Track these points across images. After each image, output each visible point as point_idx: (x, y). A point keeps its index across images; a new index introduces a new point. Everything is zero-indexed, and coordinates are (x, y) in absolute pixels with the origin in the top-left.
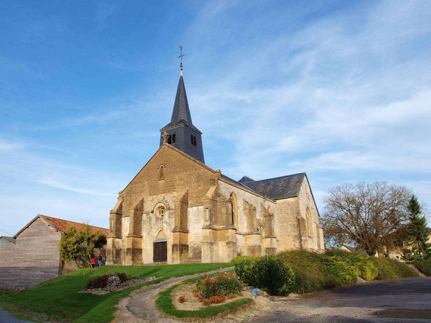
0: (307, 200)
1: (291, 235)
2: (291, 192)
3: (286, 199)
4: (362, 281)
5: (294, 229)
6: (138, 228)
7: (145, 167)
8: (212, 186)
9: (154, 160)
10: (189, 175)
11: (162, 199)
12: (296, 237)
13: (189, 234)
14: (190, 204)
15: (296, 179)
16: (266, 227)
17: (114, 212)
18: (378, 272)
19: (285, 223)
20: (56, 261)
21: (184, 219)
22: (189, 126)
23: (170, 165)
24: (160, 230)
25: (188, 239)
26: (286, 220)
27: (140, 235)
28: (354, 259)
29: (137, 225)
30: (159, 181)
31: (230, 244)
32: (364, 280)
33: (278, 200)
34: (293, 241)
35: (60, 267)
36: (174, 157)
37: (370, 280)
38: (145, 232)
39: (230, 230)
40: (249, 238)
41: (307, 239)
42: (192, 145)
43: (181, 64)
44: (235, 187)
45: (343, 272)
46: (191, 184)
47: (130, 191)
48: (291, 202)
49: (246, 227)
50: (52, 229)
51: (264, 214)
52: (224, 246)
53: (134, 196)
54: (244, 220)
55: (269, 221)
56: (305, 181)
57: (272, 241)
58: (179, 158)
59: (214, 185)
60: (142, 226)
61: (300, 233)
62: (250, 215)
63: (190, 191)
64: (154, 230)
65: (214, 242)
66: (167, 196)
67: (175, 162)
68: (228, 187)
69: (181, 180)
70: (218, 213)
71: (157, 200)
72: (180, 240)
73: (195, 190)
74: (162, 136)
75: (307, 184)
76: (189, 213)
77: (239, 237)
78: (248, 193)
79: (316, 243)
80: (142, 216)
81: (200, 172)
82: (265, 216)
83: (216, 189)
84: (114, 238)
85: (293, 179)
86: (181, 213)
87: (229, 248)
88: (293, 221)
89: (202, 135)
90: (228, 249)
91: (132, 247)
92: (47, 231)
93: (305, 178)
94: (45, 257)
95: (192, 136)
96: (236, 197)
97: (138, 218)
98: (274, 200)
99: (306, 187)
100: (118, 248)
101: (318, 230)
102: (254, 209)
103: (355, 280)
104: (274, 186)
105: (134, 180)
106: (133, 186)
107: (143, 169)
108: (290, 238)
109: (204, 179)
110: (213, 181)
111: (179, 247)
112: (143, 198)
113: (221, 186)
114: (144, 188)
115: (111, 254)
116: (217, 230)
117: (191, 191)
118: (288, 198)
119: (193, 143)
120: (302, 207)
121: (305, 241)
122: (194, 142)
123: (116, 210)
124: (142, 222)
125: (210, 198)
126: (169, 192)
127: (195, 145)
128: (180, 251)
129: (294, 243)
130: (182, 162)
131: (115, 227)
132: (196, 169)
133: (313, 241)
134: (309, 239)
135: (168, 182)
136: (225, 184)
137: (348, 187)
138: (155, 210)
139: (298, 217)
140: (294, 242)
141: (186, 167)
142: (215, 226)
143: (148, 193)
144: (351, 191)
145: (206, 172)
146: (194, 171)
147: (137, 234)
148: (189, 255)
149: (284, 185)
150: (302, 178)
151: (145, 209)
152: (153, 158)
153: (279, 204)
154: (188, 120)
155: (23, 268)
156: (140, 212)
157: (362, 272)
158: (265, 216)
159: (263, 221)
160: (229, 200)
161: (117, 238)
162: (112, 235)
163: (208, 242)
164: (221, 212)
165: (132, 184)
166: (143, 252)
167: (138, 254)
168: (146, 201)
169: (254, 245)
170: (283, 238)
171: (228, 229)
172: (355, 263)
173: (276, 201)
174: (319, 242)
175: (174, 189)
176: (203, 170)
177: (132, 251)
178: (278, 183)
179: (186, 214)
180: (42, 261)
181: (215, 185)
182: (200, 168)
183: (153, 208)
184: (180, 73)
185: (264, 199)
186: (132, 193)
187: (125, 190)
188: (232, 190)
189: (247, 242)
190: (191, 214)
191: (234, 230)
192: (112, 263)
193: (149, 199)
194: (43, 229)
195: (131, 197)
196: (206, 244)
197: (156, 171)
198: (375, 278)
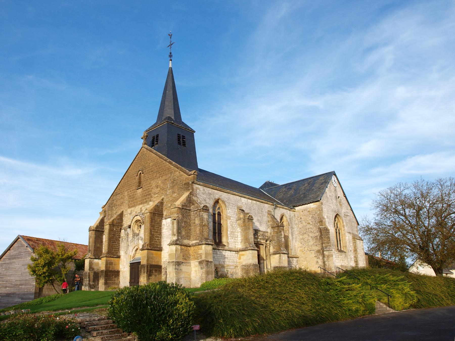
1: (313, 250)
3: (306, 205)
6: (115, 246)
7: (125, 175)
8: (186, 191)
9: (134, 166)
10: (165, 180)
11: (139, 211)
12: (318, 251)
13: (163, 252)
14: (165, 216)
15: (322, 180)
16: (274, 240)
17: (92, 229)
18: (416, 297)
19: (306, 235)
20: (32, 286)
22: (175, 123)
24: (136, 248)
25: (162, 258)
26: (306, 231)
27: (118, 255)
28: (380, 280)
30: (138, 190)
31: (203, 264)
32: (392, 309)
33: (297, 206)
34: (315, 257)
35: (35, 293)
36: (151, 161)
37: (400, 308)
38: (123, 250)
39: (204, 246)
40: (243, 255)
43: (171, 53)
44: (223, 192)
45: (348, 300)
46: (166, 191)
47: (112, 204)
48: (313, 208)
49: (240, 241)
50: (30, 250)
51: (271, 224)
52: (197, 267)
54: (238, 232)
55: (277, 233)
56: (333, 181)
57: (281, 258)
58: (156, 161)
60: (120, 244)
61: (322, 246)
62: (244, 226)
63: (165, 200)
64: (131, 248)
65: (183, 261)
68: (210, 192)
69: (157, 187)
70: (192, 225)
71: (135, 212)
72: (148, 260)
73: (170, 198)
75: (336, 185)
77: (229, 254)
78: (245, 199)
79: (351, 259)
80: (120, 232)
81: (175, 176)
82: (272, 227)
83: (189, 195)
84: (92, 258)
85: (319, 181)
86: (151, 227)
87: (202, 268)
88: (315, 232)
89: (194, 134)
90: (200, 269)
91: (106, 269)
92: (25, 253)
94: (23, 282)
96: (225, 205)
97: (115, 235)
98: (292, 207)
100: (97, 270)
101: (355, 242)
102: (250, 218)
103: (372, 309)
104: (296, 190)
105: (116, 191)
106: (114, 198)
107: (124, 178)
108: (312, 253)
109: (179, 184)
110: (187, 186)
111: (146, 268)
112: (123, 212)
113: (198, 191)
114: (124, 199)
115: (88, 277)
116: (190, 246)
117: (166, 200)
118: (309, 203)
119: (180, 143)
120: (326, 214)
121: (328, 256)
122: (181, 142)
123: (95, 226)
125: (177, 206)
127: (184, 145)
128: (147, 273)
129: (316, 260)
130: (159, 166)
131: (93, 246)
132: (172, 172)
135: (145, 190)
136: (205, 188)
137: (402, 188)
138: (132, 225)
140: (316, 258)
142: (186, 242)
143: (127, 205)
144: (406, 192)
145: (182, 175)
146: (169, 175)
147: (112, 254)
148: (162, 277)
149: (307, 188)
150: (329, 178)
151: (124, 224)
152: (133, 164)
153: (298, 211)
155: (4, 295)
156: (118, 228)
157: (388, 297)
159: (270, 234)
160: (204, 208)
162: (89, 255)
163: (173, 262)
164: (195, 223)
166: (121, 274)
167: (113, 277)
169: (248, 263)
170: (304, 253)
171: (201, 245)
172: (379, 286)
173: (295, 208)
175: (151, 198)
176: (178, 173)
177: (105, 274)
179: (159, 228)
180: (20, 287)
182: (175, 171)
184: (172, 65)
185: (274, 206)
186: (113, 206)
187: (107, 204)
188: (217, 195)
189: (241, 260)
190: (165, 228)
191: (211, 246)
192: (88, 288)
193: (128, 212)
194: (23, 251)
195: (112, 211)
196: (172, 264)
197: (135, 179)
198: (411, 306)
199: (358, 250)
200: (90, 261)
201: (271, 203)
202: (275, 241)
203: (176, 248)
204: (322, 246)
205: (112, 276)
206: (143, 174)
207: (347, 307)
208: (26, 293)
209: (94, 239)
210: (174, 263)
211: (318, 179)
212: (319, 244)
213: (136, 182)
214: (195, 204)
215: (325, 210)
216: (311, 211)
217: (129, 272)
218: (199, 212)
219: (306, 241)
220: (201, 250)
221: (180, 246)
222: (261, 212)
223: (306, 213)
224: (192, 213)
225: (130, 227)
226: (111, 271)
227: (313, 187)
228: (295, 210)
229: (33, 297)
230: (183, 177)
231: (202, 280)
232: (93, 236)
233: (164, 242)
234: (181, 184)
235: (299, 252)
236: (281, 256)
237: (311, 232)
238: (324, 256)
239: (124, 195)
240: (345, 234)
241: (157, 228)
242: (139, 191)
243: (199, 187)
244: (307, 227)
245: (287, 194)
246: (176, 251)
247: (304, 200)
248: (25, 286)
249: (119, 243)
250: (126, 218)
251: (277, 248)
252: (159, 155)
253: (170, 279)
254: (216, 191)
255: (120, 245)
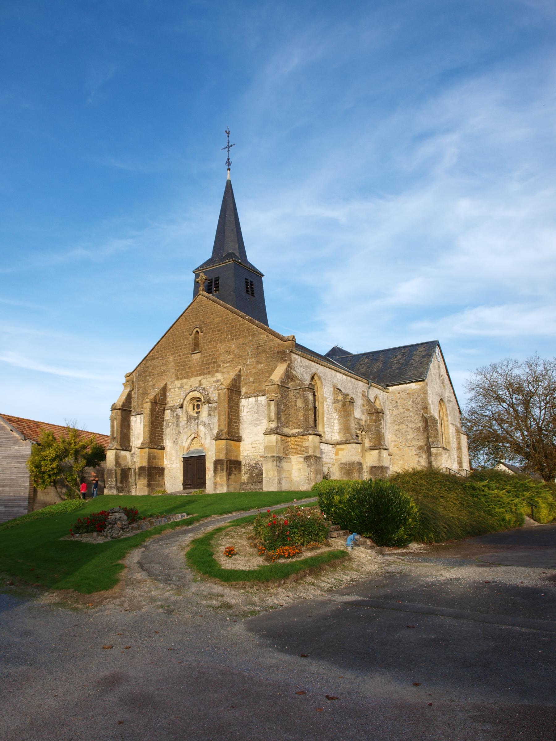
0: (440, 387)
1: (413, 446)
2: (413, 372)
3: (405, 385)
4: (533, 524)
5: (417, 435)
6: (158, 433)
7: (169, 332)
8: (281, 362)
11: (197, 385)
12: (421, 448)
13: (242, 443)
14: (244, 393)
17: (118, 407)
19: (403, 425)
21: (233, 418)
22: (242, 263)
23: (210, 329)
24: (193, 437)
25: (241, 451)
26: (404, 420)
28: (520, 487)
29: (155, 428)
30: (193, 355)
31: (310, 460)
32: (536, 523)
34: (416, 455)
36: (217, 315)
37: (545, 521)
38: (168, 439)
39: (311, 437)
40: (342, 449)
41: (440, 453)
42: (247, 294)
43: (228, 159)
44: (319, 364)
45: (500, 508)
46: (245, 359)
47: (145, 372)
48: (414, 389)
49: (338, 431)
51: (367, 410)
53: (150, 380)
55: (376, 421)
57: (381, 455)
59: (284, 361)
60: (164, 430)
61: (428, 441)
62: (344, 411)
64: (183, 437)
65: (284, 456)
66: (205, 380)
67: (219, 323)
68: (307, 364)
69: (229, 353)
70: (291, 408)
71: (189, 387)
72: (226, 453)
73: (252, 370)
74: (197, 280)
75: (440, 359)
76: (242, 408)
78: (341, 375)
79: (454, 459)
80: (164, 413)
81: (261, 340)
82: (369, 414)
85: (418, 352)
86: (229, 408)
87: (308, 466)
88: (417, 421)
89: (263, 278)
90: (306, 467)
92: (8, 439)
93: (437, 350)
95: (246, 279)
96: (321, 381)
97: (158, 417)
99: (439, 364)
100: (125, 466)
101: (459, 438)
102: (351, 401)
104: (384, 363)
105: (151, 354)
106: (149, 363)
107: (166, 335)
108: (411, 450)
109: (268, 352)
110: (282, 355)
111: (225, 464)
112: (166, 384)
113: (296, 362)
115: (114, 476)
116: (289, 437)
117: (245, 372)
118: (409, 383)
119: (249, 291)
121: (436, 455)
122: (250, 290)
123: (121, 404)
124: (165, 423)
125: (277, 383)
126: (209, 373)
127: (253, 294)
128: (226, 471)
129: (417, 459)
130: (231, 323)
131: (119, 432)
133: (449, 455)
134: (443, 452)
136: (302, 359)
137: (511, 366)
138: (185, 403)
139: (425, 415)
140: (417, 456)
141: (237, 332)
142: (286, 430)
143: (174, 376)
144: (516, 372)
145: (272, 340)
149: (402, 361)
151: (169, 402)
152: (182, 317)
153: (393, 392)
154: (240, 253)
156: (161, 407)
158: (369, 414)
159: (366, 422)
161: (123, 450)
163: (273, 457)
164: (296, 406)
165: (148, 360)
166: (166, 472)
167: (157, 476)
168: (170, 389)
169: (350, 461)
172: (521, 493)
174: (460, 457)
175: (218, 368)
176: (265, 336)
177: (148, 472)
178: (391, 358)
179: (236, 410)
181: (285, 361)
183: (182, 400)
185: (369, 384)
186: (147, 376)
187: (136, 371)
188: (313, 369)
189: (339, 457)
190: (246, 410)
193: (176, 385)
194: (3, 437)
196: (271, 459)
199: (462, 448)
200: (116, 453)
201: (366, 381)
202: (373, 431)
203: (277, 438)
204: (428, 441)
205: (156, 475)
206: (201, 332)
207: (499, 517)
208: (12, 498)
209: (120, 422)
210: (275, 458)
211: (416, 350)
212: (423, 438)
213: (189, 344)
214: (296, 380)
215: (430, 392)
216: (411, 393)
217: (182, 470)
218: (302, 391)
219: (403, 433)
220: (307, 443)
221: (280, 436)
222: (356, 392)
223: (404, 395)
224: (291, 393)
225: (181, 407)
226: (155, 468)
227: (412, 361)
228: (388, 391)
229: (25, 503)
230: (274, 343)
231: (309, 481)
232: (119, 417)
233: (245, 429)
234: (271, 351)
235: (392, 447)
236: (382, 453)
237: (411, 421)
238: (429, 454)
239: (166, 361)
240: (448, 425)
241: (235, 409)
242: (195, 356)
243: (297, 357)
244: (406, 414)
245: (372, 368)
246: (277, 442)
247: (402, 378)
248: (10, 488)
249: (163, 429)
250: (171, 394)
251: (375, 442)
252: (231, 308)
253: (268, 479)
254: (312, 363)
255: (163, 432)
